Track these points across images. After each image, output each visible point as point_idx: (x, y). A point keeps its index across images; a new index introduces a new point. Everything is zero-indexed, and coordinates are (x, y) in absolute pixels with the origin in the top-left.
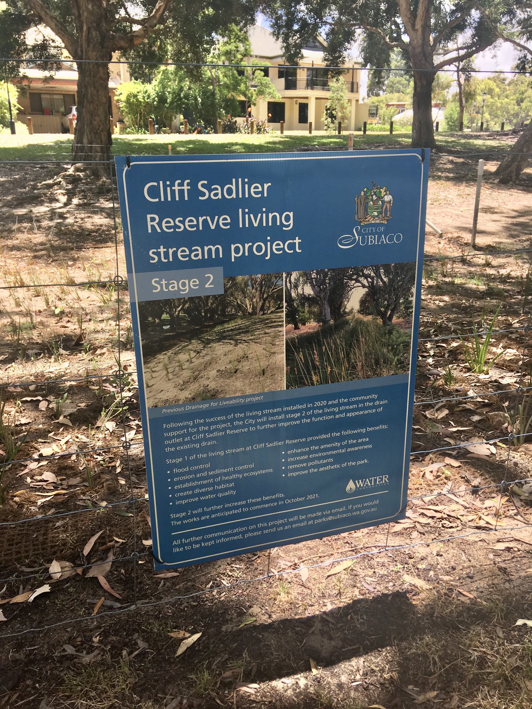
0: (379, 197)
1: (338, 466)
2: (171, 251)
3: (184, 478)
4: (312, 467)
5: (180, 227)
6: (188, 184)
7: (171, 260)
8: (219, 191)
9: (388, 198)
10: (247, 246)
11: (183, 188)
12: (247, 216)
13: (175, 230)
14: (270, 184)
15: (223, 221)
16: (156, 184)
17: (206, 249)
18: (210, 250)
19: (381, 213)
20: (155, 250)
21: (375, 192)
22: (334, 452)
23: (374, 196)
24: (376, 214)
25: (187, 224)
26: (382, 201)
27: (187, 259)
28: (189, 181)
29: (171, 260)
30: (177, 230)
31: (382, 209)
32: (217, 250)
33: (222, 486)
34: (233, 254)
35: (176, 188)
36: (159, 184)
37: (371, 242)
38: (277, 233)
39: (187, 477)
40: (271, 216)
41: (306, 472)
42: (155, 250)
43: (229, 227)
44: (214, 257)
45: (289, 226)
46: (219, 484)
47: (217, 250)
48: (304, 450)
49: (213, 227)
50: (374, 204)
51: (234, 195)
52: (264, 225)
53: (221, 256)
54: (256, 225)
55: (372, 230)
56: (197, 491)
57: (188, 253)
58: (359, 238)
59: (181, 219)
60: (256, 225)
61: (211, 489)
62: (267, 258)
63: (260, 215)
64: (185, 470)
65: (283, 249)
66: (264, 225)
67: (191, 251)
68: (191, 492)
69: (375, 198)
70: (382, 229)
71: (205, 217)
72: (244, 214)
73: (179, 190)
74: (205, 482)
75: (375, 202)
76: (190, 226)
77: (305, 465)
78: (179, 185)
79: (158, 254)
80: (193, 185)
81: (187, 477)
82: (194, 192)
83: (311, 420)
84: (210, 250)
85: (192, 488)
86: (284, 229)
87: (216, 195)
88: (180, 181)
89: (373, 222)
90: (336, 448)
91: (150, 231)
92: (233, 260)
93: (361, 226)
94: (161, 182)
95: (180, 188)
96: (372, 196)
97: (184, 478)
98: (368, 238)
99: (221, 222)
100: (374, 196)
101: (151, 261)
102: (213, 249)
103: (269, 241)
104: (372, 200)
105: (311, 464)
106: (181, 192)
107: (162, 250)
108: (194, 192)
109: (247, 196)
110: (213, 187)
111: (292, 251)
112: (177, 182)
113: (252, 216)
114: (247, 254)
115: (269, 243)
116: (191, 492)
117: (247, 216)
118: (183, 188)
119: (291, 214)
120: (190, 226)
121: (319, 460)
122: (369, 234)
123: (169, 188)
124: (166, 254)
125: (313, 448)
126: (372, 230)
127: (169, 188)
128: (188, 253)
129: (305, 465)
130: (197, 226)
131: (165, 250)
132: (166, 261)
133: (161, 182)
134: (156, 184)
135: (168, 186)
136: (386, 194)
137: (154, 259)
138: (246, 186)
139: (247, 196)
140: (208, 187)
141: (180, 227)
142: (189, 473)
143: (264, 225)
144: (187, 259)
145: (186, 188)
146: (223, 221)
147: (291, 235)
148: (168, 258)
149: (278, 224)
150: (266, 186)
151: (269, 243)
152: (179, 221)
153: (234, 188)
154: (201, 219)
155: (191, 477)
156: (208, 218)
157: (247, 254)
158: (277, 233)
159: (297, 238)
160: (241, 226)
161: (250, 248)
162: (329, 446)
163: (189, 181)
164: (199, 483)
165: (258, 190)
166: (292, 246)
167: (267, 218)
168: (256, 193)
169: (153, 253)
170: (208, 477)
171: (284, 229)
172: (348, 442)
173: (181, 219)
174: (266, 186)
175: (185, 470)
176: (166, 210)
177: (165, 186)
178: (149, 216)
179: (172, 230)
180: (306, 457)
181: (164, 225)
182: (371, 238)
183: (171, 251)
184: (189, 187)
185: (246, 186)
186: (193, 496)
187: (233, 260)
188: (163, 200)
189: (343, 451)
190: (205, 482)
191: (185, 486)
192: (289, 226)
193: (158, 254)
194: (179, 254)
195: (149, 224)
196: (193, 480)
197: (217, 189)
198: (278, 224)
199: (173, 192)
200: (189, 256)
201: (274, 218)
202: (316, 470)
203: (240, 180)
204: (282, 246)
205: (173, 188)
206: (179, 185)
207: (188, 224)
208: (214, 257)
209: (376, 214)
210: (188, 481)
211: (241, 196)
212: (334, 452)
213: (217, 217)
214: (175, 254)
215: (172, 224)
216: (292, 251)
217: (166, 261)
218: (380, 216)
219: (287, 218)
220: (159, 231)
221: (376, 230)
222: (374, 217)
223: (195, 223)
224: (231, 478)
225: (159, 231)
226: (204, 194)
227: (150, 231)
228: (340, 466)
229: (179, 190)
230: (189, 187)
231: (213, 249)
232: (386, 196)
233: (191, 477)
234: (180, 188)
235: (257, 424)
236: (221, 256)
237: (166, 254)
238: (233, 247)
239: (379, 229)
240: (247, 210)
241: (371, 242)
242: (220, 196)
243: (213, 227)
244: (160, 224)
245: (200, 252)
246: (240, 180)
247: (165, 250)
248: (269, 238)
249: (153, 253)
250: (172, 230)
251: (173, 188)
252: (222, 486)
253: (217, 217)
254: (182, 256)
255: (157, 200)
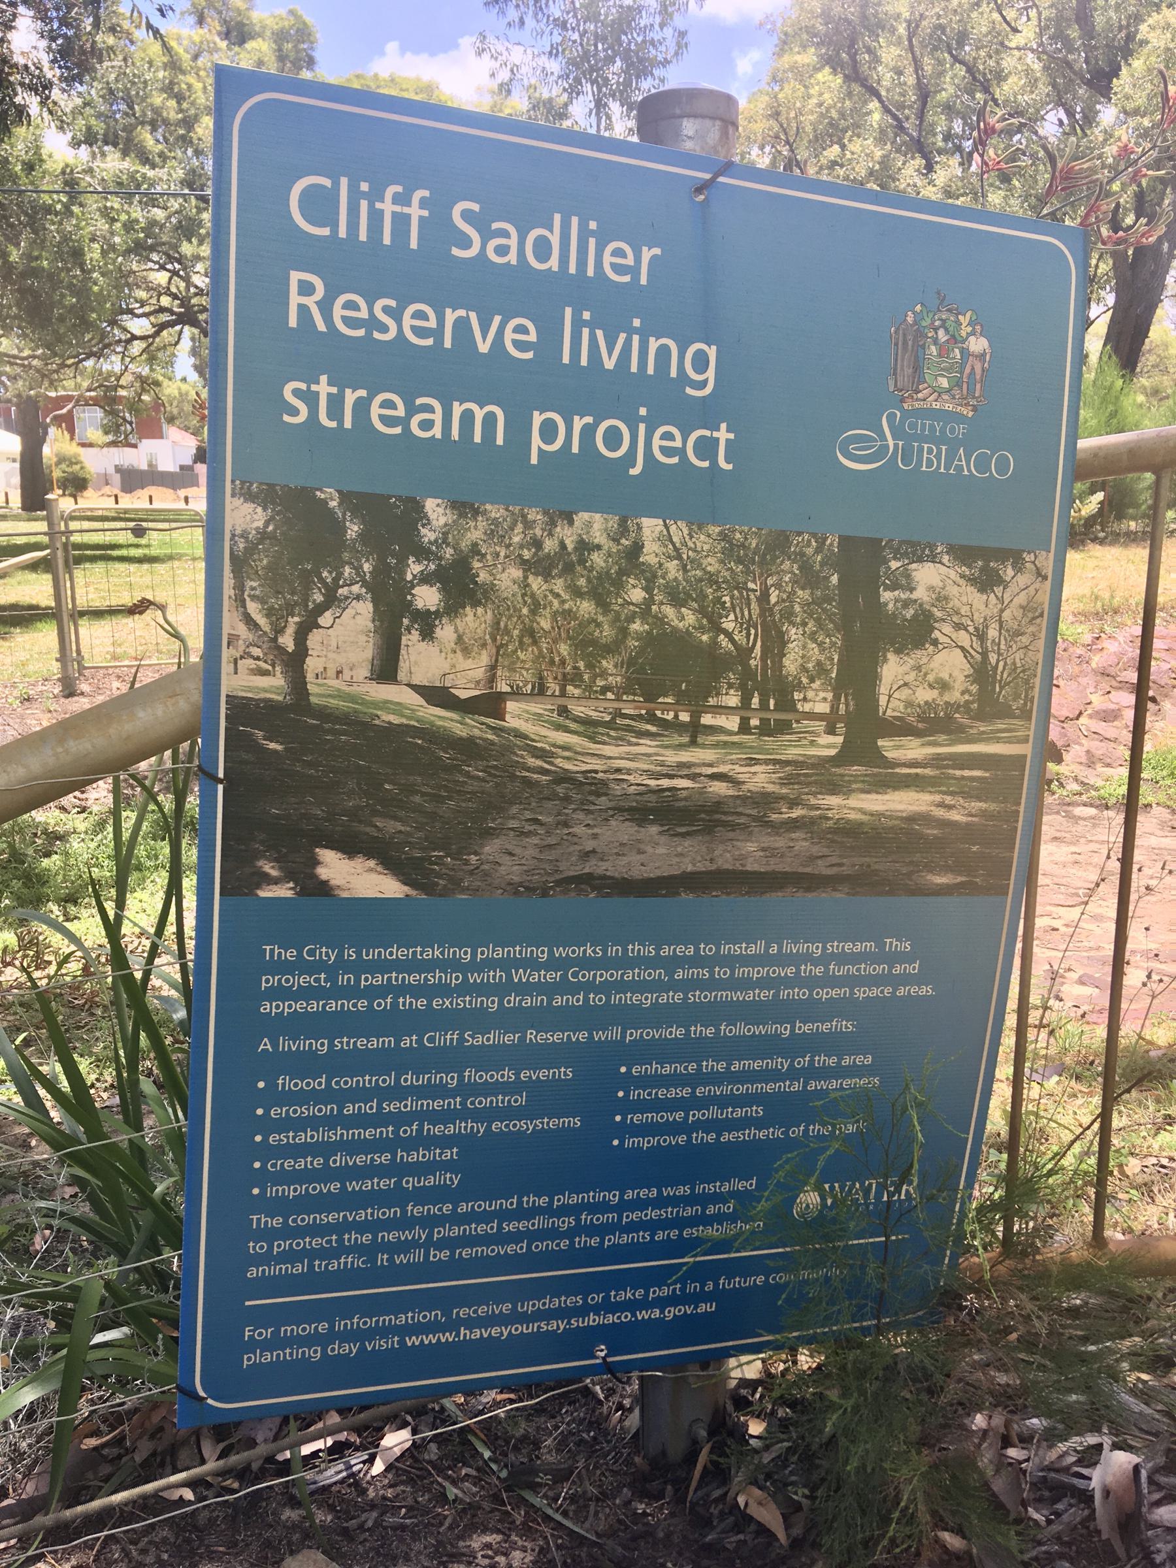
0: (953, 337)
1: (779, 1134)
2: (350, 397)
3: (303, 1111)
4: (698, 1125)
5: (384, 329)
6: (423, 204)
7: (348, 424)
8: (513, 242)
9: (978, 344)
10: (578, 423)
11: (406, 210)
12: (586, 332)
13: (369, 334)
14: (657, 251)
15: (516, 335)
16: (328, 183)
17: (457, 409)
18: (468, 417)
19: (958, 384)
20: (303, 386)
21: (944, 321)
22: (769, 1088)
23: (941, 332)
24: (944, 383)
25: (407, 321)
26: (962, 351)
27: (398, 430)
28: (427, 193)
29: (348, 424)
30: (376, 335)
31: (962, 373)
32: (490, 419)
33: (417, 1156)
34: (536, 441)
35: (388, 207)
36: (336, 184)
37: (930, 463)
38: (667, 401)
39: (314, 1111)
40: (654, 344)
41: (682, 1139)
42: (303, 386)
43: (529, 355)
44: (478, 439)
45: (703, 384)
46: (411, 1144)
47: (490, 419)
48: (681, 1069)
49: (484, 347)
50: (940, 355)
51: (554, 263)
52: (634, 369)
53: (500, 441)
54: (609, 364)
55: (932, 427)
56: (338, 1160)
57: (401, 412)
58: (896, 446)
59: (393, 303)
60: (609, 364)
61: (385, 1158)
62: (633, 472)
63: (623, 336)
64: (314, 1084)
65: (682, 452)
66: (634, 369)
67: (411, 410)
68: (318, 1162)
69: (942, 336)
70: (961, 430)
71: (462, 313)
72: (578, 324)
73: (394, 214)
74: (368, 1134)
75: (944, 351)
76: (416, 330)
77: (679, 1116)
78: (397, 199)
79: (311, 399)
80: (439, 208)
81: (314, 1111)
82: (438, 227)
83: (718, 1030)
84: (468, 417)
85: (325, 1149)
86: (689, 391)
87: (502, 251)
88: (399, 189)
89: (936, 405)
90: (773, 1075)
91: (293, 322)
92: (534, 460)
93: (902, 410)
94: (344, 181)
95: (398, 209)
96: (936, 330)
97: (303, 1111)
98: (921, 450)
99: (509, 336)
100: (941, 332)
101: (286, 418)
102: (479, 414)
103: (642, 419)
104: (935, 341)
105: (699, 1115)
106: (402, 221)
107: (324, 388)
108: (438, 227)
109: (590, 272)
110: (495, 226)
111: (706, 464)
112: (391, 190)
113: (599, 334)
114: (575, 449)
115: (642, 427)
116: (318, 1162)
117: (586, 332)
118: (406, 210)
119: (712, 352)
120: (416, 330)
121: (722, 1107)
122: (923, 439)
123: (364, 205)
124: (336, 404)
125: (708, 1065)
126: (932, 427)
127: (364, 205)
128: (401, 412)
129: (679, 1116)
130: (438, 333)
131: (334, 390)
132: (334, 424)
133: (344, 181)
134: (328, 183)
135: (364, 195)
136: (973, 333)
137: (295, 412)
138: (592, 242)
139: (590, 272)
140: (480, 222)
141: (384, 329)
142: (325, 1097)
143: (634, 369)
144: (398, 430)
145: (415, 212)
146: (516, 335)
147: (706, 413)
148: (341, 421)
149: (674, 373)
150: (647, 254)
151: (642, 427)
152: (386, 310)
153: (555, 240)
154: (450, 316)
155: (326, 1110)
156: (473, 316)
157: (575, 449)
158: (667, 401)
159: (723, 426)
160: (566, 359)
161: (588, 432)
162: (756, 1065)
163: (427, 193)
164: (348, 1135)
165: (757, 1111)
166: (707, 448)
167: (645, 352)
168: (616, 268)
169: (296, 393)
170: (379, 1120)
171: (689, 391)
172: (812, 1061)
173: (393, 303)
174: (647, 254)
175: (314, 1084)
176: (348, 266)
177: (355, 196)
178: (295, 276)
179: (361, 333)
180: (685, 1092)
181: (338, 312)
182: (930, 451)
183: (350, 397)
184: (426, 213)
185: (592, 242)
186: (326, 1174)
187: (534, 460)
188: (342, 233)
189: (797, 1087)
190: (368, 1134)
191: (302, 1138)
192: (704, 384)
193: (311, 399)
194: (375, 411)
195: (295, 299)
196: (331, 1122)
197: (507, 235)
198: (674, 373)
199: (376, 217)
200: (405, 422)
201: (663, 352)
202: (711, 1138)
203: (575, 220)
204: (678, 443)
205: (378, 205)
206: (397, 199)
207: (410, 323)
208: (478, 439)
209: (944, 383)
210: (313, 1123)
211: (572, 270)
212: (769, 1088)
213: (497, 319)
214: (362, 407)
215: (364, 314)
216: (706, 464)
217: (334, 424)
218: (956, 392)
219: (701, 362)
220: (321, 327)
221: (943, 431)
222: (938, 392)
223: (432, 323)
224: (451, 1129)
225: (321, 327)
226: (466, 243)
227: (293, 322)
228: (785, 1133)
229: (394, 214)
230: (426, 213)
231: (479, 414)
232: (972, 339)
233: (326, 1110)
234: (398, 209)
235: (429, 1243)
236: (500, 441)
237: (336, 404)
238: (538, 418)
239: (952, 431)
240: (586, 315)
241: (930, 463)
242: (512, 258)
243: (484, 347)
244: (326, 306)
245: (438, 417)
246: (575, 220)
247: (334, 390)
248: (643, 411)
249: (296, 393)
250: (361, 333)
251: (378, 205)
252: (417, 1156)
253: (497, 319)
254: (382, 418)
255: (326, 231)
